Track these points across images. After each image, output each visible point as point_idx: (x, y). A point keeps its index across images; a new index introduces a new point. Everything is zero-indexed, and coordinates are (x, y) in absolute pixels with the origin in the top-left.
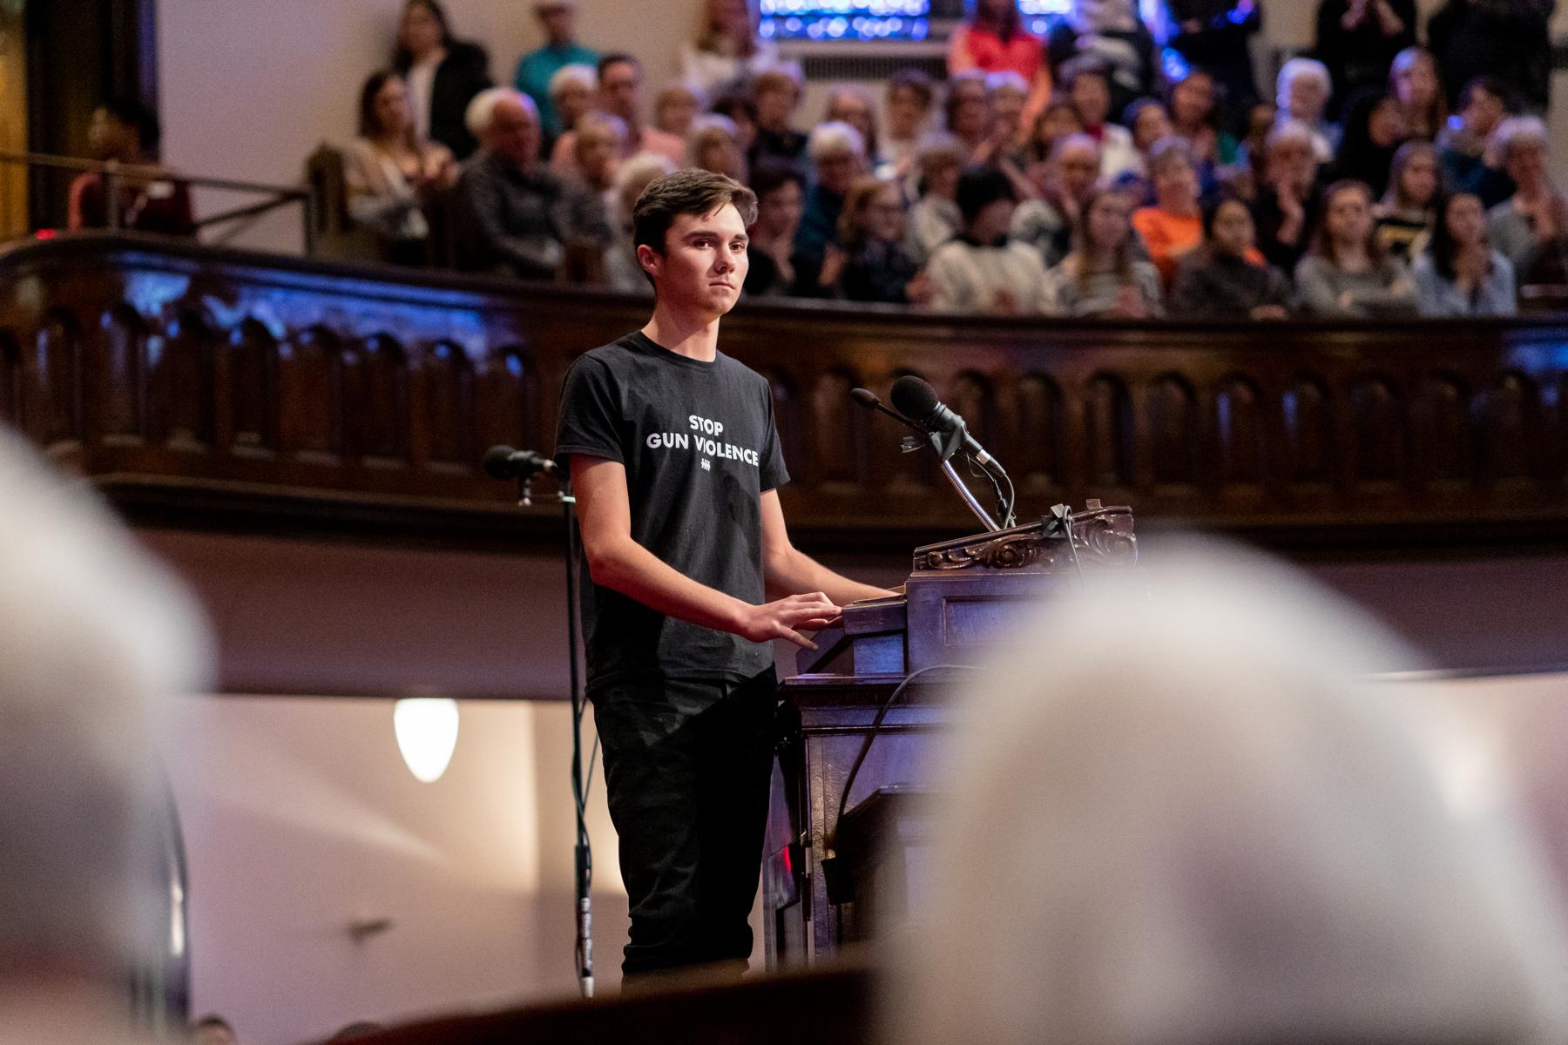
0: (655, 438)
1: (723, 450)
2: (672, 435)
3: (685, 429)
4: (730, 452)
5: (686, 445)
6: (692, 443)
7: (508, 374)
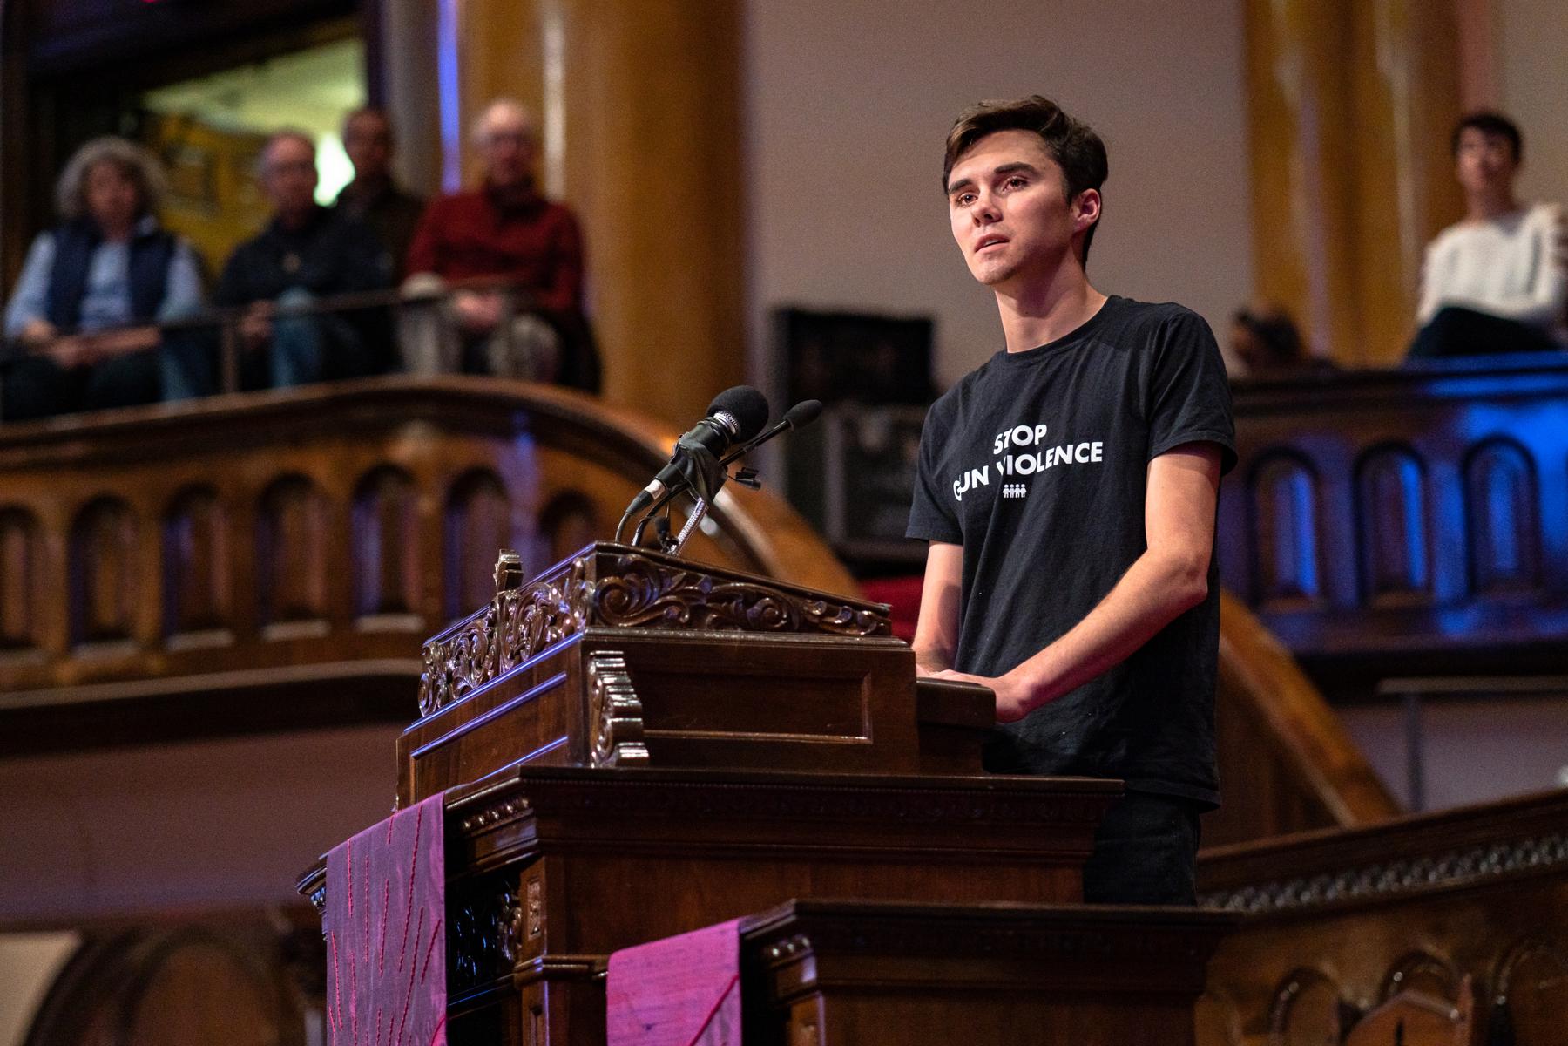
0: (957, 488)
1: (1043, 463)
5: (985, 481)
6: (993, 473)
7: (724, 430)
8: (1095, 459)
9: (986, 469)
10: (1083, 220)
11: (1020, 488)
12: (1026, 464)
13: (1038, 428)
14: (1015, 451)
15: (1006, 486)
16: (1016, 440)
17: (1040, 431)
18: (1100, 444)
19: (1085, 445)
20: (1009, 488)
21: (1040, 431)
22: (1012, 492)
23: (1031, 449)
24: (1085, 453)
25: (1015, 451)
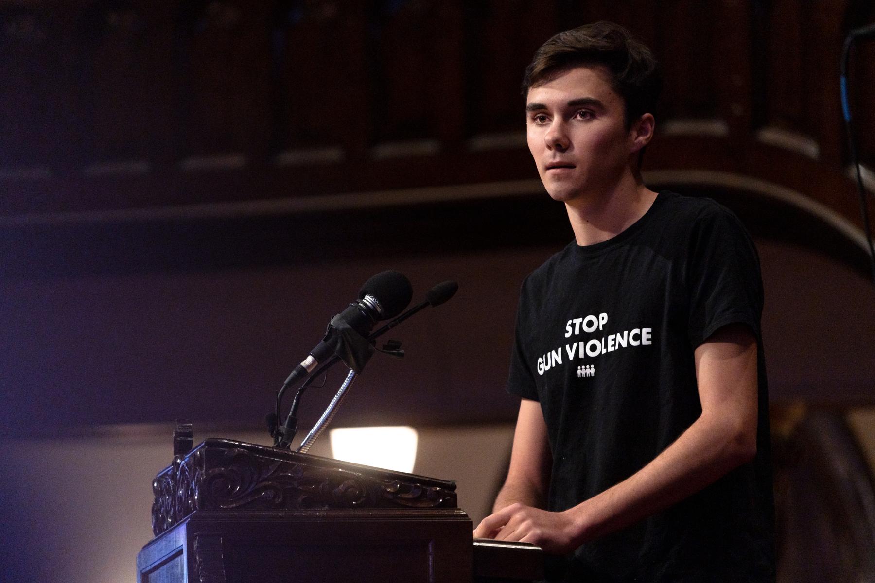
0: (540, 363)
1: (606, 347)
2: (549, 354)
3: (559, 342)
4: (613, 343)
6: (565, 355)
8: (645, 342)
9: (560, 350)
10: (640, 143)
11: (590, 368)
12: (593, 348)
13: (601, 315)
14: (584, 337)
15: (579, 367)
16: (585, 328)
17: (603, 318)
18: (650, 330)
19: (636, 331)
20: (581, 369)
21: (603, 318)
22: (583, 372)
23: (598, 335)
24: (637, 337)
25: (584, 337)
